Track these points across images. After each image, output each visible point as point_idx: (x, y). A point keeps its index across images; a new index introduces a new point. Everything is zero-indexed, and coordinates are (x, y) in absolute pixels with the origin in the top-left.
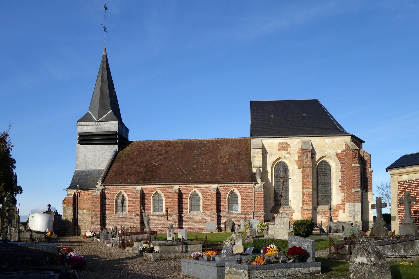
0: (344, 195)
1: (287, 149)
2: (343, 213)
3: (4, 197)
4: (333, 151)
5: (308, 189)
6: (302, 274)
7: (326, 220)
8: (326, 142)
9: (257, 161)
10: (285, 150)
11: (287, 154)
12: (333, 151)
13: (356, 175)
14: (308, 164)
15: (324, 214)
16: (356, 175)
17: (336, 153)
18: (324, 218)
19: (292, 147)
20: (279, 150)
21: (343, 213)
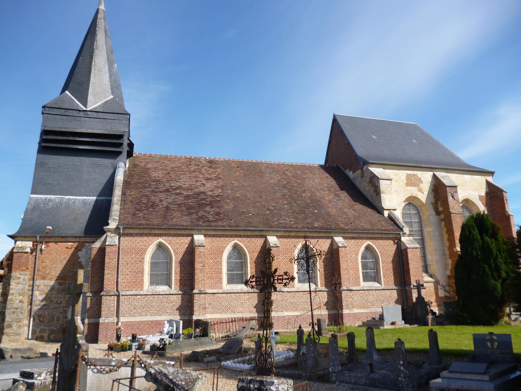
1: (419, 185)
10: (415, 186)
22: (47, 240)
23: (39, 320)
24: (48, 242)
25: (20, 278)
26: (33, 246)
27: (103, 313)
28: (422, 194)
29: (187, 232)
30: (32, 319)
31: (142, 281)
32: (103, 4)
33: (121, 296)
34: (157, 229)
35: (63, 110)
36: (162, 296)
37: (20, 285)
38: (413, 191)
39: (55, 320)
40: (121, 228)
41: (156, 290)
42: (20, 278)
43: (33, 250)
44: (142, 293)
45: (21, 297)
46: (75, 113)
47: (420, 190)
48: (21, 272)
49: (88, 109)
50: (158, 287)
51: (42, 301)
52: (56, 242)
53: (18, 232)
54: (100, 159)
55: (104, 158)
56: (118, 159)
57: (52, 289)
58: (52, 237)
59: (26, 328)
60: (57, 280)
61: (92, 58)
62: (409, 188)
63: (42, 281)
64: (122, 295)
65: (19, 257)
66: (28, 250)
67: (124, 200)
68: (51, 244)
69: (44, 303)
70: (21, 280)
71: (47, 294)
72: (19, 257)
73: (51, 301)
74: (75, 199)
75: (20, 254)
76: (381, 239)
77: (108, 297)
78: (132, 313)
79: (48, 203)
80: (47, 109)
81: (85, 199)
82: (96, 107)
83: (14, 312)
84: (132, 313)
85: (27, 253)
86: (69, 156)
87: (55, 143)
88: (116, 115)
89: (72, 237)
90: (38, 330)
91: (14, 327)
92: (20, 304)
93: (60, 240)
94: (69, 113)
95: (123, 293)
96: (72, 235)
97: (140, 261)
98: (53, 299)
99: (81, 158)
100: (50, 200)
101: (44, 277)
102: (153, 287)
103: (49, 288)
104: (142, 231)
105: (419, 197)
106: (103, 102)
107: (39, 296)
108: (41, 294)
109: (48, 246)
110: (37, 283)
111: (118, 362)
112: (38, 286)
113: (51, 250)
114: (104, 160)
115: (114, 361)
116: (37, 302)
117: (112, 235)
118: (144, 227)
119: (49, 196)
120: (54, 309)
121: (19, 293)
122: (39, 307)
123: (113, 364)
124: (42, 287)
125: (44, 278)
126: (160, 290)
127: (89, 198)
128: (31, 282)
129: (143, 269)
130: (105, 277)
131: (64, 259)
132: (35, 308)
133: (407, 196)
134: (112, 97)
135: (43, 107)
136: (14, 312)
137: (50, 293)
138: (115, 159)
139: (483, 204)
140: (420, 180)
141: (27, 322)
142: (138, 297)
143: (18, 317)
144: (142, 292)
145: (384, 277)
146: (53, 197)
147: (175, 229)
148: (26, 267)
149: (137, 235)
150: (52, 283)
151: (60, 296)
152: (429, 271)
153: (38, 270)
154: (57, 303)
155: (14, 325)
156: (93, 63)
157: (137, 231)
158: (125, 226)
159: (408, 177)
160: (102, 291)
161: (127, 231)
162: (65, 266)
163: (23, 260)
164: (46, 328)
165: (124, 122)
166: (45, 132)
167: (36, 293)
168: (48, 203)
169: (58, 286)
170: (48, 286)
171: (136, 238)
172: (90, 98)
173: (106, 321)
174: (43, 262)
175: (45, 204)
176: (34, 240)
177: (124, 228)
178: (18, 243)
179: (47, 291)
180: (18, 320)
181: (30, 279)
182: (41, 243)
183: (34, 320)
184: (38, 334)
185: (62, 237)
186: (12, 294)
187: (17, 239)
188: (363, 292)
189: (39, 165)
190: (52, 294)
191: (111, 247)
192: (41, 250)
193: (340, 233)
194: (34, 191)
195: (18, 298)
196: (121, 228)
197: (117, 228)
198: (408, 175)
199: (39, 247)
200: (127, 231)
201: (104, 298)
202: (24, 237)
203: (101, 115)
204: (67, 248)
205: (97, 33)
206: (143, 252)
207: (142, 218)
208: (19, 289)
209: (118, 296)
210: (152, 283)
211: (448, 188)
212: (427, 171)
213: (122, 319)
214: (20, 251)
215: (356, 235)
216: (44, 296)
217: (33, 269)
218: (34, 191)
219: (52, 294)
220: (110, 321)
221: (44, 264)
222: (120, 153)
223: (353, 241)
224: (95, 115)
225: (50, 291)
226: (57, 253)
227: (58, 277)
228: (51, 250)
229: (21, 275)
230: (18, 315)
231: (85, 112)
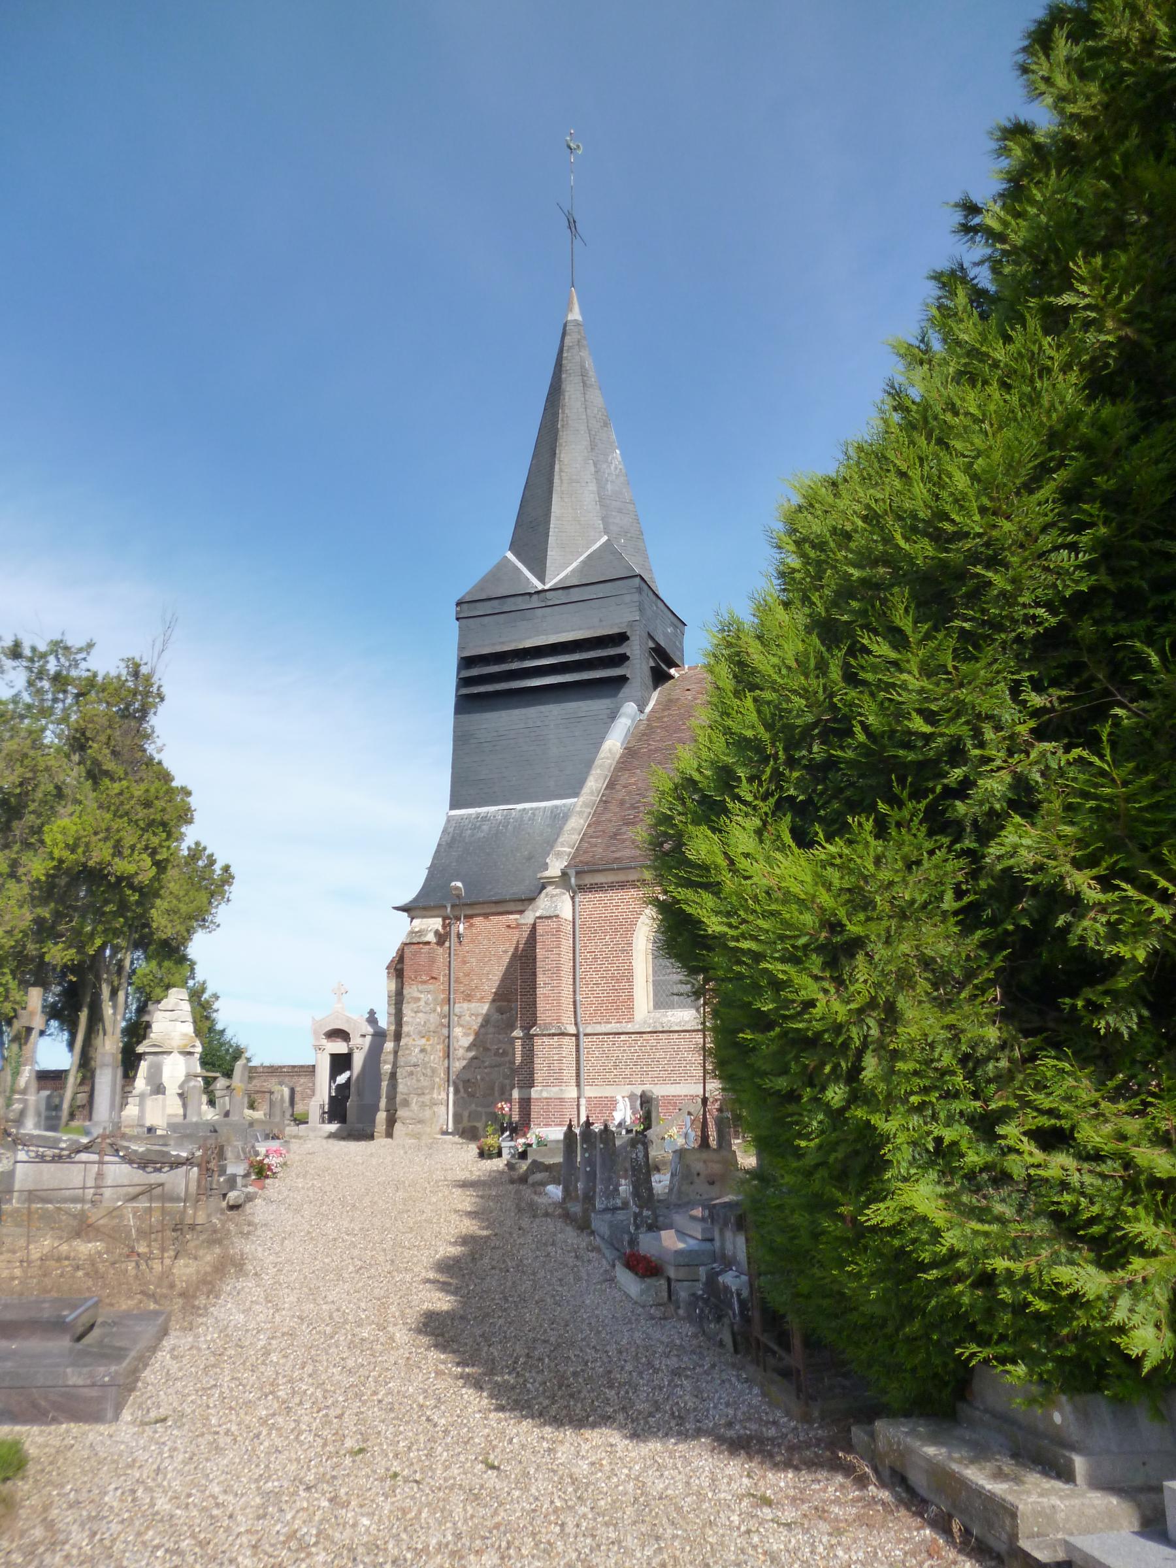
22: (469, 912)
23: (466, 1091)
24: (471, 917)
25: (419, 999)
26: (444, 926)
27: (538, 1076)
30: (451, 1089)
31: (631, 998)
33: (581, 1036)
35: (496, 602)
36: (676, 1035)
37: (420, 1015)
39: (496, 1094)
40: (572, 872)
41: (665, 1020)
42: (419, 999)
43: (442, 938)
44: (629, 1027)
45: (423, 1041)
46: (521, 603)
48: (420, 987)
49: (546, 587)
50: (670, 1013)
51: (469, 1049)
52: (486, 916)
53: (415, 900)
54: (581, 704)
55: (591, 698)
56: (621, 695)
57: (486, 1021)
58: (479, 903)
59: (443, 1108)
60: (494, 1001)
61: (553, 454)
63: (465, 1005)
64: (586, 1035)
65: (415, 954)
66: (431, 937)
67: (606, 802)
68: (477, 921)
69: (472, 1054)
70: (422, 1003)
71: (477, 1034)
72: (415, 954)
73: (487, 1049)
74: (536, 809)
75: (416, 947)
77: (545, 1039)
78: (610, 1076)
79: (480, 827)
80: (465, 606)
81: (556, 807)
82: (566, 577)
83: (411, 1073)
84: (610, 1076)
85: (428, 943)
86: (517, 707)
87: (490, 683)
88: (601, 585)
89: (514, 901)
90: (466, 1114)
91: (414, 1106)
92: (422, 1056)
93: (494, 910)
94: (509, 605)
95: (589, 1031)
96: (517, 897)
97: (623, 951)
98: (488, 1046)
99: (542, 708)
100: (485, 818)
101: (469, 995)
102: (658, 1014)
103: (480, 1020)
104: (621, 877)
106: (582, 558)
107: (463, 1038)
108: (466, 1035)
109: (472, 925)
110: (458, 1008)
111: (71, 1145)
112: (460, 1017)
113: (479, 934)
114: (589, 702)
115: (65, 1141)
116: (461, 1052)
117: (558, 891)
118: (620, 866)
119: (483, 810)
120: (491, 1067)
121: (420, 1032)
122: (464, 1063)
123: (63, 1145)
124: (467, 1018)
125: (468, 998)
126: (672, 1019)
127: (564, 801)
128: (446, 1008)
129: (630, 970)
130: (539, 991)
131: (505, 952)
132: (458, 1065)
134: (605, 538)
135: (458, 604)
136: (411, 1073)
137: (483, 1030)
138: (615, 695)
141: (443, 1095)
142: (623, 1037)
143: (420, 1085)
144: (630, 1025)
146: (492, 809)
147: (613, 869)
148: (427, 975)
149: (612, 886)
150: (485, 1008)
151: (501, 1037)
153: (457, 981)
154: (496, 1054)
155: (414, 1100)
156: (557, 467)
157: (610, 878)
158: (579, 869)
160: (535, 1024)
161: (588, 880)
162: (507, 969)
163: (423, 960)
164: (479, 1109)
165: (627, 598)
166: (467, 662)
167: (458, 1031)
168: (480, 827)
169: (496, 1016)
170: (477, 1015)
171: (610, 894)
172: (552, 554)
173: (545, 1095)
174: (464, 962)
175: (475, 828)
176: (442, 912)
177: (577, 873)
178: (416, 922)
179: (476, 1027)
180: (420, 1091)
181: (443, 1000)
182: (458, 919)
183: (456, 1092)
184: (466, 1123)
185: (497, 903)
186: (408, 1035)
187: (414, 913)
189: (461, 740)
190: (487, 1034)
191: (547, 922)
192: (459, 935)
194: (453, 806)
195: (417, 1043)
196: (572, 872)
197: (564, 874)
199: (454, 930)
200: (588, 880)
201: (538, 1041)
202: (425, 908)
203: (575, 595)
204: (509, 926)
205: (563, 386)
206: (629, 927)
207: (628, 843)
208: (419, 1024)
209: (577, 1036)
210: (658, 1005)
213: (589, 1092)
214: (414, 941)
216: (471, 1038)
217: (446, 979)
218: (453, 806)
219: (487, 1034)
220: (552, 1095)
221: (467, 967)
222: (623, 680)
224: (561, 597)
225: (482, 1026)
226: (489, 940)
227: (495, 993)
228: (479, 934)
229: (421, 992)
230: (418, 1081)
231: (542, 595)
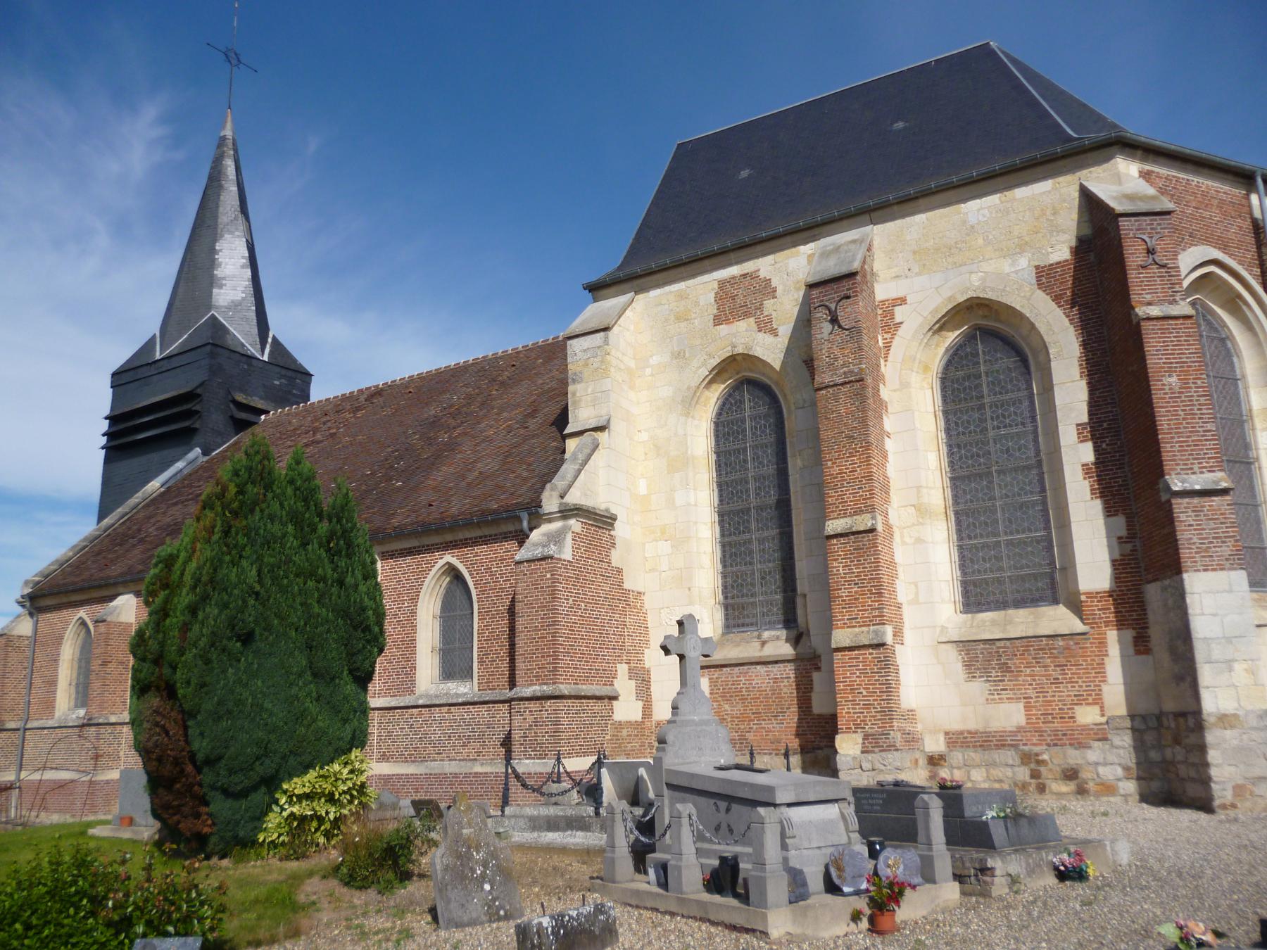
0: (1130, 527)
1: (760, 307)
2: (1138, 652)
3: (490, 892)
4: (1014, 263)
5: (856, 513)
6: (290, 893)
7: (1021, 706)
8: (964, 222)
9: (589, 398)
10: (747, 315)
11: (761, 335)
12: (1014, 263)
13: (1174, 380)
14: (844, 365)
15: (1005, 669)
16: (1174, 380)
17: (1037, 267)
18: (1004, 695)
19: (779, 293)
20: (718, 321)
21: (1138, 652)
28: (769, 339)
29: (505, 528)
32: (229, 125)
34: (507, 518)
38: (743, 336)
44: (51, 723)
47: (766, 326)
62: (724, 329)
76: (484, 540)
105: (759, 352)
133: (714, 362)
139: (1057, 299)
140: (767, 289)
142: (46, 732)
145: (481, 661)
152: (800, 619)
159: (725, 292)
188: (415, 711)
193: (125, 583)
198: (722, 284)
211: (1123, 222)
212: (795, 245)
215: (414, 543)
223: (409, 560)
